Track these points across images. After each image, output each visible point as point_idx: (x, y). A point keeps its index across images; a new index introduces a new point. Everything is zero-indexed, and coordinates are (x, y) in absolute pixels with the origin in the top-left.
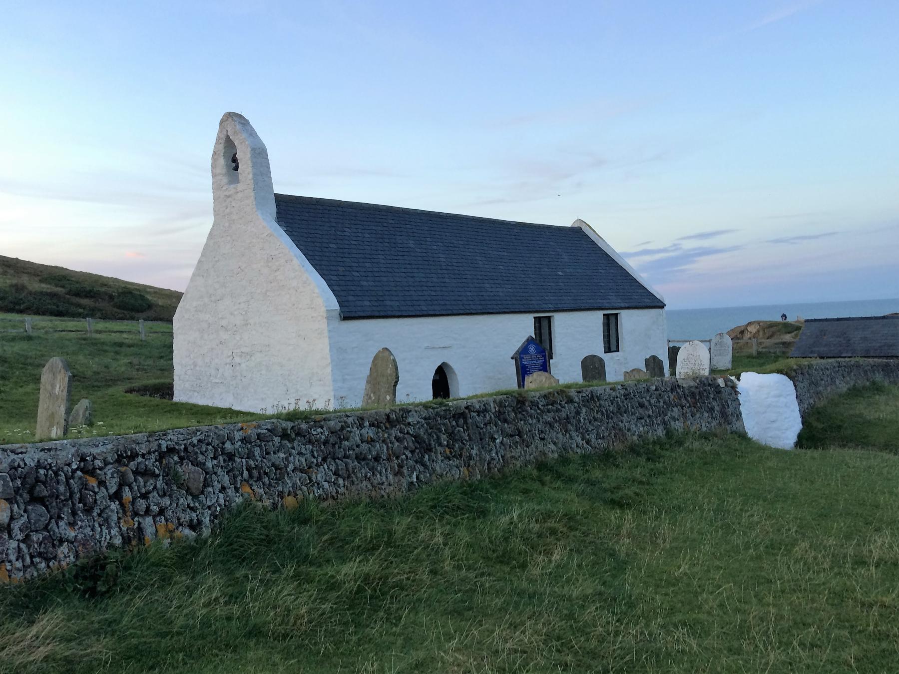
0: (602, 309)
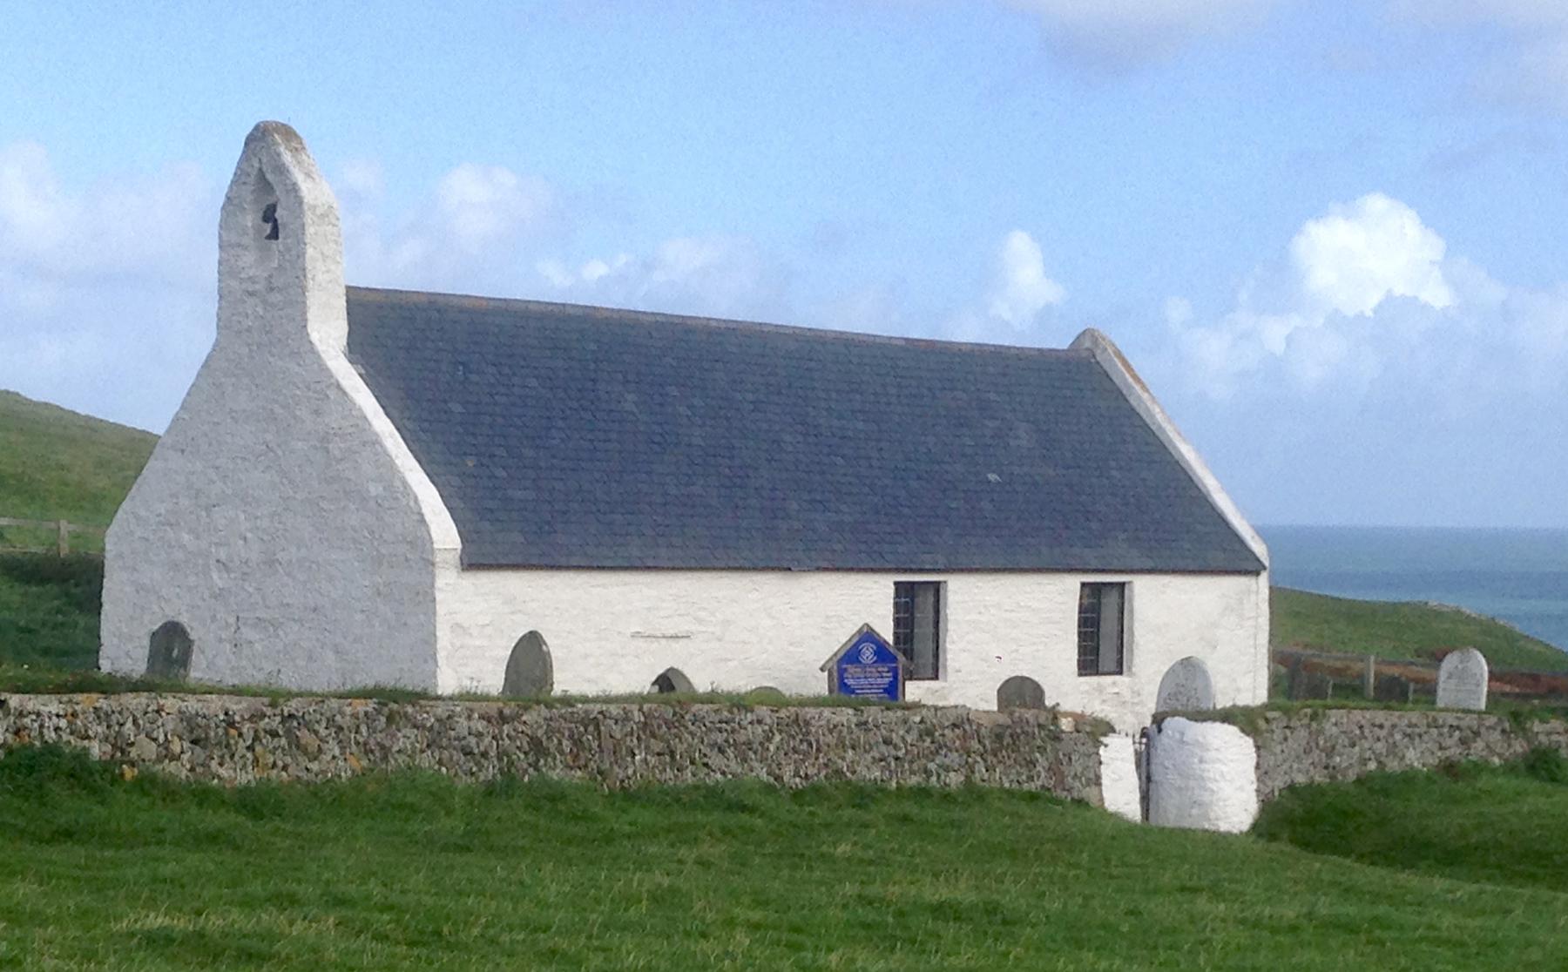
0: (898, 570)
